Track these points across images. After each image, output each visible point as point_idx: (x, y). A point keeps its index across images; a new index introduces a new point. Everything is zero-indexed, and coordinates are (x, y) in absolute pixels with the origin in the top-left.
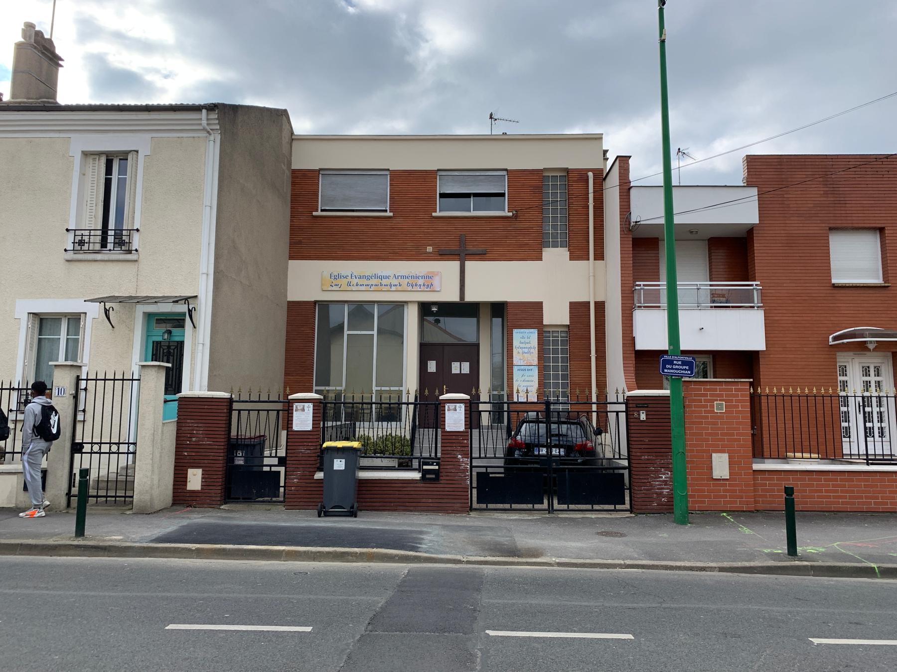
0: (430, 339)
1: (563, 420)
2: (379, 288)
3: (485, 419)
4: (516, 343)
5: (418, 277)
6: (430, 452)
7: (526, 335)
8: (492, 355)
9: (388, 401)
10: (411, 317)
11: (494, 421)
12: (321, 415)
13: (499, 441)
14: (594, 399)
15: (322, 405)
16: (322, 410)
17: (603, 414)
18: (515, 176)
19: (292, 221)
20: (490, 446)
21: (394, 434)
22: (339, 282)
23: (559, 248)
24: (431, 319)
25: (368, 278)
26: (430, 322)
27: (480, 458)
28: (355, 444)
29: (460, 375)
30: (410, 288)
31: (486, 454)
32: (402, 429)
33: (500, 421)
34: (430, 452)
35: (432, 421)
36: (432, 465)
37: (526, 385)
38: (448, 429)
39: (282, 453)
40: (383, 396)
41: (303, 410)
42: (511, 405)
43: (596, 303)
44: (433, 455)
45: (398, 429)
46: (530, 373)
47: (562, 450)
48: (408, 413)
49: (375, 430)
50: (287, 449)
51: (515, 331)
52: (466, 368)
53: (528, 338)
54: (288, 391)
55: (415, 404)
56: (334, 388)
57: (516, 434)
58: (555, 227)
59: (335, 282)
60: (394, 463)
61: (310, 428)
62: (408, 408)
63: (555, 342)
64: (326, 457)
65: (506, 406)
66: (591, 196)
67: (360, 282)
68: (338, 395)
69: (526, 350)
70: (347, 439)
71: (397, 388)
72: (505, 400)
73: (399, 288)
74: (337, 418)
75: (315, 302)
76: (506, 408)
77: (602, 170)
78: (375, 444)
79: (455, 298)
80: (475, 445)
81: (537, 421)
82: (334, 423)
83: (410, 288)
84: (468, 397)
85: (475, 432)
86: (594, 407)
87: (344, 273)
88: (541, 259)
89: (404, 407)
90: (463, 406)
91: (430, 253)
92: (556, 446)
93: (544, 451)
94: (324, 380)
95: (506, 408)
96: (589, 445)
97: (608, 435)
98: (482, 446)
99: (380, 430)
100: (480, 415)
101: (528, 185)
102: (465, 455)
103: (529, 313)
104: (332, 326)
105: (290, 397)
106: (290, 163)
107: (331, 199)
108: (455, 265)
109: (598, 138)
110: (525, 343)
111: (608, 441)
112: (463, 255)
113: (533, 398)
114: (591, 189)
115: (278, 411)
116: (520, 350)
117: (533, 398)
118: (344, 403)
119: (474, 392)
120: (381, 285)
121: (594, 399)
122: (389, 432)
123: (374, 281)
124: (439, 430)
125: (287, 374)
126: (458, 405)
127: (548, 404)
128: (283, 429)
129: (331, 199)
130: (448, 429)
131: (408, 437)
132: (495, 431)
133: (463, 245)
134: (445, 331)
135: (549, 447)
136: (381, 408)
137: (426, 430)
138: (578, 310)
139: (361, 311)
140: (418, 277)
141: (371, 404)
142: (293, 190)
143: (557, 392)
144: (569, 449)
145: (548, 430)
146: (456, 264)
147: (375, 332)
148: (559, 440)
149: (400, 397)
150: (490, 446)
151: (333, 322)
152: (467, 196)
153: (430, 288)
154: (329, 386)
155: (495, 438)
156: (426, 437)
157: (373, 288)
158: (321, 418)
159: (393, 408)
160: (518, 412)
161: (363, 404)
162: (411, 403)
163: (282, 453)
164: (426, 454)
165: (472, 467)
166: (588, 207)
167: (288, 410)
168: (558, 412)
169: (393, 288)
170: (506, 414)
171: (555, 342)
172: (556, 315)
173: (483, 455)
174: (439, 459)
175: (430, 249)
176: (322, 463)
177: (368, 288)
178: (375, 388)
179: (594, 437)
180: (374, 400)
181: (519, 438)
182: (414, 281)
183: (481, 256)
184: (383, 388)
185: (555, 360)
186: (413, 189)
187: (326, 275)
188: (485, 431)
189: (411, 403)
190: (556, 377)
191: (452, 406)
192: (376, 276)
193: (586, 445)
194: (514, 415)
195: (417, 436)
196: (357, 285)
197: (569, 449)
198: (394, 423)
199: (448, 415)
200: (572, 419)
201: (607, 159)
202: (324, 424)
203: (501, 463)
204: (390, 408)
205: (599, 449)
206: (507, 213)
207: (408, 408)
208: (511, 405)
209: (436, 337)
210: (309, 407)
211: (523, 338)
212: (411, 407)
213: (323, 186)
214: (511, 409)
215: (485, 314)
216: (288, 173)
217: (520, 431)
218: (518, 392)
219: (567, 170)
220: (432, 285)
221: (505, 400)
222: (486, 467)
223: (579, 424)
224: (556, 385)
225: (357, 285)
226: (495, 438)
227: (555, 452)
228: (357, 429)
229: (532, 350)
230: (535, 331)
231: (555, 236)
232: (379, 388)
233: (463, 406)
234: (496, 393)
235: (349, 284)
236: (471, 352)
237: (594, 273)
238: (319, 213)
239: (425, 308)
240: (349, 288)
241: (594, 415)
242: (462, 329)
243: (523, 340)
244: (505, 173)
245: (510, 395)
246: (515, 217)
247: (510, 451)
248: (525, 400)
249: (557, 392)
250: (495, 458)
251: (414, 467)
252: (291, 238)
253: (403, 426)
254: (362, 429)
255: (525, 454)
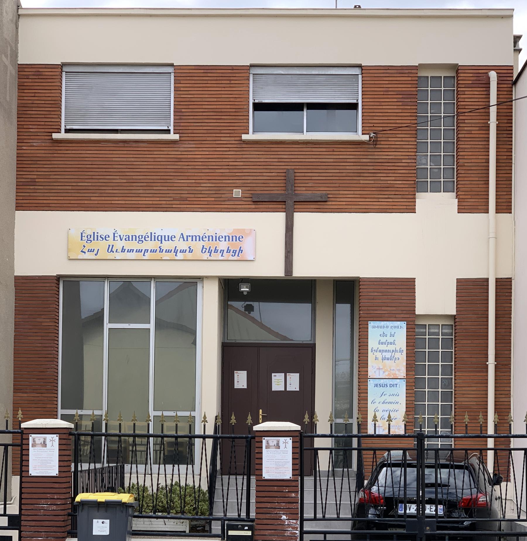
0: (236, 337)
1: (442, 462)
2: (158, 255)
3: (324, 461)
4: (373, 343)
5: (218, 239)
6: (239, 511)
7: (388, 331)
8: (335, 362)
9: (173, 433)
10: (208, 305)
11: (335, 464)
12: (71, 453)
13: (346, 495)
14: (491, 431)
15: (72, 438)
16: (72, 445)
17: (503, 453)
18: (375, 77)
19: (19, 148)
20: (331, 501)
21: (183, 484)
22: (94, 245)
23: (442, 193)
24: (239, 305)
25: (141, 239)
26: (237, 310)
27: (315, 519)
28: (125, 498)
29: (285, 394)
30: (206, 256)
31: (324, 513)
32: (195, 475)
33: (347, 464)
34: (239, 511)
35: (241, 463)
36: (242, 529)
37: (387, 409)
38: (266, 475)
39: (14, 509)
40: (165, 425)
41: (44, 445)
42: (363, 440)
43: (498, 280)
44: (243, 515)
45: (190, 477)
46: (393, 390)
47: (440, 507)
48: (203, 451)
49: (155, 476)
50: (21, 504)
51: (371, 324)
52: (293, 382)
53: (392, 335)
54: (20, 416)
55: (215, 438)
56: (90, 412)
57: (372, 483)
58: (435, 159)
59: (89, 246)
60: (184, 526)
61: (55, 472)
62: (204, 443)
63: (434, 343)
64: (81, 516)
65: (355, 441)
66: (493, 111)
67: (128, 245)
68: (96, 423)
69: (388, 355)
70: (112, 490)
71: (187, 414)
72: (355, 432)
73: (189, 256)
74: (95, 457)
75: (58, 278)
76: (355, 444)
77: (510, 68)
78: (155, 497)
79: (274, 269)
80: (309, 499)
81: (403, 464)
82: (92, 466)
83: (206, 256)
84: (297, 427)
85: (309, 481)
86: (491, 443)
87: (102, 232)
88: (413, 211)
89: (198, 442)
90: (289, 441)
91: (237, 199)
92: (431, 502)
93: (412, 509)
94: (75, 399)
95: (355, 444)
96: (482, 499)
97: (511, 485)
98: (319, 501)
99: (162, 477)
100: (316, 454)
101: (395, 88)
102: (292, 515)
103: (395, 297)
104: (83, 317)
105: (23, 425)
106: (15, 54)
107: (80, 111)
108: (278, 218)
109: (506, 16)
110: (386, 341)
111: (511, 494)
112: (290, 202)
113: (399, 429)
114: (493, 100)
115: (6, 446)
116: (379, 355)
117: (399, 429)
118: (106, 435)
119: (307, 419)
120: (161, 251)
121: (491, 431)
122: (176, 479)
123: (149, 245)
124: (253, 479)
125: (16, 390)
126: (282, 439)
127: (420, 438)
128: (14, 474)
129: (80, 111)
130: (266, 475)
131: (205, 487)
132: (338, 480)
133: (291, 188)
134: (262, 326)
135: (421, 502)
136: (162, 443)
137: (233, 477)
138: (471, 291)
139: (129, 292)
140: (218, 239)
141: (109, 466)
142: (20, 98)
143: (435, 419)
144: (451, 506)
145: (420, 478)
146: (280, 217)
147: (152, 326)
148: (436, 493)
149: (191, 428)
150: (331, 501)
151: (87, 307)
152: (298, 107)
153: (237, 253)
154: (81, 408)
155: (338, 490)
156: (233, 488)
157: (148, 256)
158: (72, 458)
159: (182, 443)
160: (375, 450)
161: (135, 436)
162: (209, 437)
163: (14, 509)
164: (232, 514)
165: (302, 532)
166: (488, 127)
167: (21, 445)
168: (437, 451)
169: (180, 256)
170: (355, 453)
171: (434, 343)
172: (436, 300)
173: (319, 515)
174: (252, 521)
175: (237, 193)
176: (74, 525)
177: (140, 255)
178: (152, 413)
179: (489, 488)
180: (151, 432)
181: (374, 489)
182: (213, 244)
183: (319, 204)
184: (166, 413)
185: (434, 370)
186: (211, 94)
187: (75, 235)
188: (324, 479)
189: (209, 437)
190: (434, 396)
191: (273, 441)
192: (153, 237)
193: (477, 499)
194: (368, 456)
195: (218, 486)
196: (123, 250)
197: (451, 506)
198: (183, 467)
199: (266, 454)
200: (456, 461)
201: (520, 50)
202: (76, 467)
203: (347, 526)
204: (177, 444)
205: (496, 505)
206: (360, 136)
207: (204, 443)
208: (363, 440)
209: (247, 333)
210: (53, 440)
211: (384, 335)
212: (209, 442)
213: (71, 96)
214: (363, 446)
215: (324, 299)
216: (12, 71)
217: (376, 478)
218: (375, 419)
219: (456, 68)
220: (241, 251)
221: (355, 432)
222: (325, 533)
223: (467, 468)
224: (434, 409)
225: (123, 250)
226: (338, 490)
227: (430, 510)
228: (127, 476)
229: (398, 355)
230: (403, 325)
231: (435, 174)
232: (159, 413)
233: (289, 441)
234: (340, 421)
235: (110, 249)
236: (301, 357)
237: (496, 233)
238: (62, 135)
239: (229, 287)
240: (111, 256)
241: (490, 455)
242: (288, 320)
243: (383, 340)
244: (357, 71)
245: (362, 425)
246: (374, 142)
247: (360, 509)
248: (386, 432)
249: (435, 419)
250: (338, 519)
251: (214, 532)
252: (18, 176)
253: (197, 472)
254: (134, 476)
255: (386, 514)
